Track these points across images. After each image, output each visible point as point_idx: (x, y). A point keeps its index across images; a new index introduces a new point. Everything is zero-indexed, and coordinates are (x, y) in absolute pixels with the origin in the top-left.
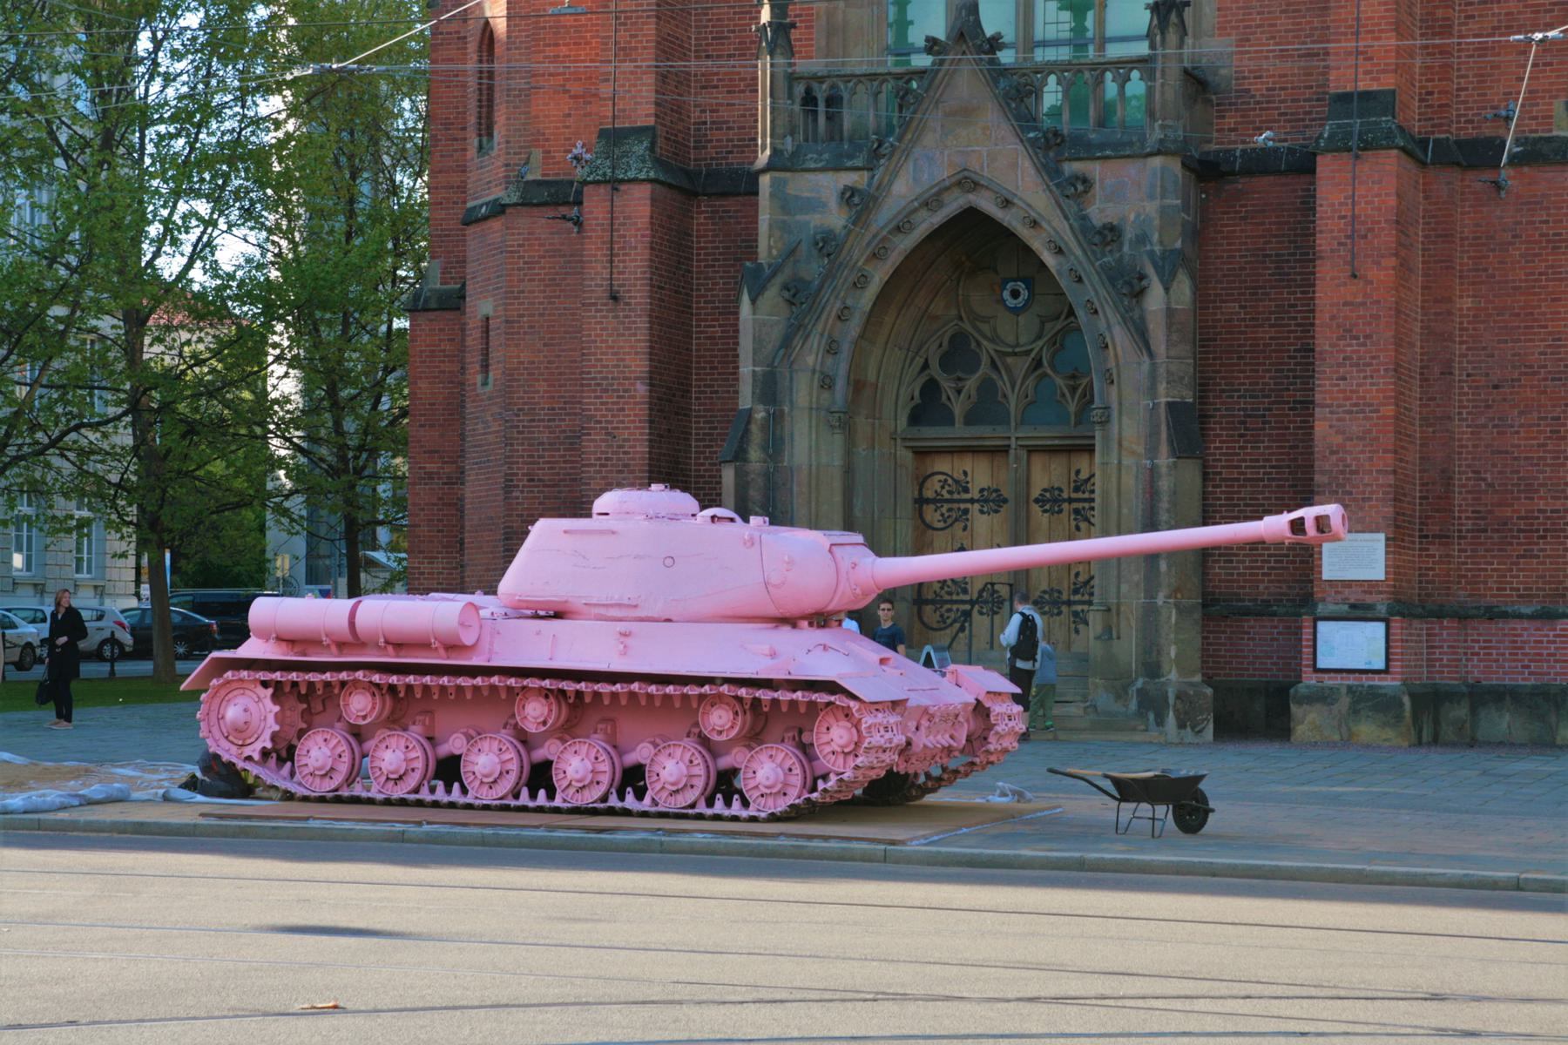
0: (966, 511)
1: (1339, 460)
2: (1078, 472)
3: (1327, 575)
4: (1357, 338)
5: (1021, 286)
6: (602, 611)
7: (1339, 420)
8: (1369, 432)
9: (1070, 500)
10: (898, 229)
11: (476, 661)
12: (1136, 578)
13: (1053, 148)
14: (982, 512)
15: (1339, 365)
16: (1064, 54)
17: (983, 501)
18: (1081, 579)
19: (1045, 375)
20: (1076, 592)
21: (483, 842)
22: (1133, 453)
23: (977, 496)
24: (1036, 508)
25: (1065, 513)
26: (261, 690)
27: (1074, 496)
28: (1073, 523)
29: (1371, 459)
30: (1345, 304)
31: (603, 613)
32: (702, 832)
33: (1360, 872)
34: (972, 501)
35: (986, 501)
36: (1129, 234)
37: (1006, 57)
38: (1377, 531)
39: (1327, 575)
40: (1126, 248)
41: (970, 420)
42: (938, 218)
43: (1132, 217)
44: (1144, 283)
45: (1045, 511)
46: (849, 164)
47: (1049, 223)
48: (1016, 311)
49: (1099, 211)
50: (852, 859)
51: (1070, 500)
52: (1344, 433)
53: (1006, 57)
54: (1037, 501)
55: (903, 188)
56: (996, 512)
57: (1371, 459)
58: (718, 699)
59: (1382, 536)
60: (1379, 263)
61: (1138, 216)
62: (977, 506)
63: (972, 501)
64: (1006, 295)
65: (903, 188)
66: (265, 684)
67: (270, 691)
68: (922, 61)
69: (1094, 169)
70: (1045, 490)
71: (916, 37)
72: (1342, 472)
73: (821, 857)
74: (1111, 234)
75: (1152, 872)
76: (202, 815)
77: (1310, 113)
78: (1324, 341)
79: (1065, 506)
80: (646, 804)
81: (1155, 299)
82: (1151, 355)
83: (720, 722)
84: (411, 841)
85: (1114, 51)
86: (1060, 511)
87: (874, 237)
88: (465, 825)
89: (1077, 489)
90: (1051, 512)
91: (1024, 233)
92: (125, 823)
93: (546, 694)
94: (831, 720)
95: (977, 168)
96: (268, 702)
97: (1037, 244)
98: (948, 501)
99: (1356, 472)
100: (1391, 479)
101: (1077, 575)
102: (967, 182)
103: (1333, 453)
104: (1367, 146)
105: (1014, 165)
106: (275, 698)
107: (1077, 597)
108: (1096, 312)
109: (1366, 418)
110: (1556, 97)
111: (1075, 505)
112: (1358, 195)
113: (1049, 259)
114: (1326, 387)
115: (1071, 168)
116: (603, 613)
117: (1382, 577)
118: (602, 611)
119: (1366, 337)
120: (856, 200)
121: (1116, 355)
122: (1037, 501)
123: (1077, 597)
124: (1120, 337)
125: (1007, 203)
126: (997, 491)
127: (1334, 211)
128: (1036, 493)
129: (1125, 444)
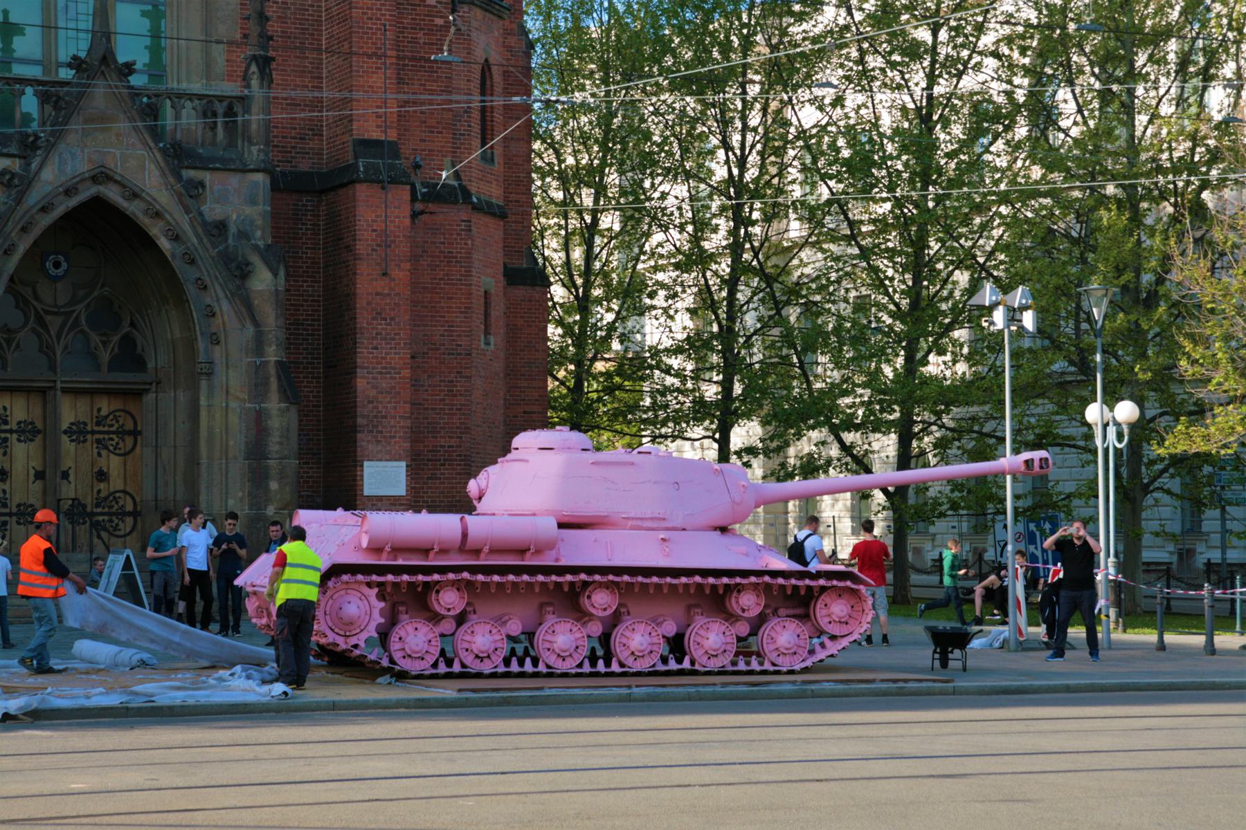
0: (5, 440)
1: (374, 408)
2: (99, 410)
3: (366, 493)
4: (385, 319)
5: (61, 258)
6: (639, 523)
7: (374, 378)
8: (394, 388)
9: (93, 432)
10: (44, 209)
11: (547, 560)
12: (240, 494)
13: (178, 156)
14: (19, 440)
15: (373, 338)
16: (34, 72)
17: (20, 432)
18: (102, 495)
19: (82, 332)
20: (98, 506)
21: (689, 698)
22: (238, 398)
23: (15, 427)
24: (65, 438)
25: (88, 444)
26: (365, 590)
27: (96, 428)
28: (96, 451)
29: (395, 408)
30: (377, 294)
31: (638, 524)
32: (828, 681)
33: (1092, 685)
34: (11, 431)
35: (23, 432)
36: (233, 229)
37: (137, 80)
38: (399, 460)
39: (366, 493)
40: (230, 241)
41: (112, 367)
42: (73, 202)
43: (234, 217)
44: (250, 268)
45: (72, 441)
46: (5, 151)
47: (170, 214)
48: (56, 279)
49: (213, 210)
50: (934, 694)
51: (93, 432)
52: (376, 388)
53: (137, 80)
54: (65, 432)
55: (50, 176)
56: (32, 440)
57: (395, 408)
58: (739, 589)
59: (404, 464)
60: (399, 266)
61: (238, 217)
62: (15, 436)
63: (11, 431)
64: (49, 265)
65: (50, 176)
66: (369, 585)
67: (376, 590)
68: (66, 74)
69: (206, 176)
70: (72, 424)
71: (64, 55)
72: (376, 417)
73: (601, 701)
74: (221, 227)
75: (1107, 691)
76: (460, 690)
77: (294, 148)
78: (363, 319)
79: (89, 437)
80: (686, 664)
81: (263, 281)
82: (256, 324)
83: (748, 603)
84: (635, 700)
85: (19, 70)
86: (85, 441)
87: (26, 213)
88: (920, 681)
89: (98, 424)
90: (78, 441)
91: (145, 221)
92: (409, 700)
93: (457, 585)
94: (828, 600)
95: (112, 166)
96: (374, 600)
97: (156, 230)
98: (113, 433)
99: (385, 417)
100: (408, 423)
101: (99, 492)
102: (102, 176)
103: (370, 402)
104: (394, 181)
105: (143, 168)
106: (381, 596)
107: (99, 510)
108: (205, 287)
109: (391, 378)
110: (445, 156)
111: (97, 436)
112: (378, 214)
113: (164, 244)
114: (364, 354)
115: (191, 174)
116: (638, 524)
117: (404, 493)
118: (639, 523)
119: (392, 319)
120: (16, 181)
121: (224, 323)
122: (65, 432)
123: (99, 510)
124: (225, 308)
125: (135, 195)
126: (32, 423)
127: (368, 226)
128: (65, 426)
129: (232, 391)
